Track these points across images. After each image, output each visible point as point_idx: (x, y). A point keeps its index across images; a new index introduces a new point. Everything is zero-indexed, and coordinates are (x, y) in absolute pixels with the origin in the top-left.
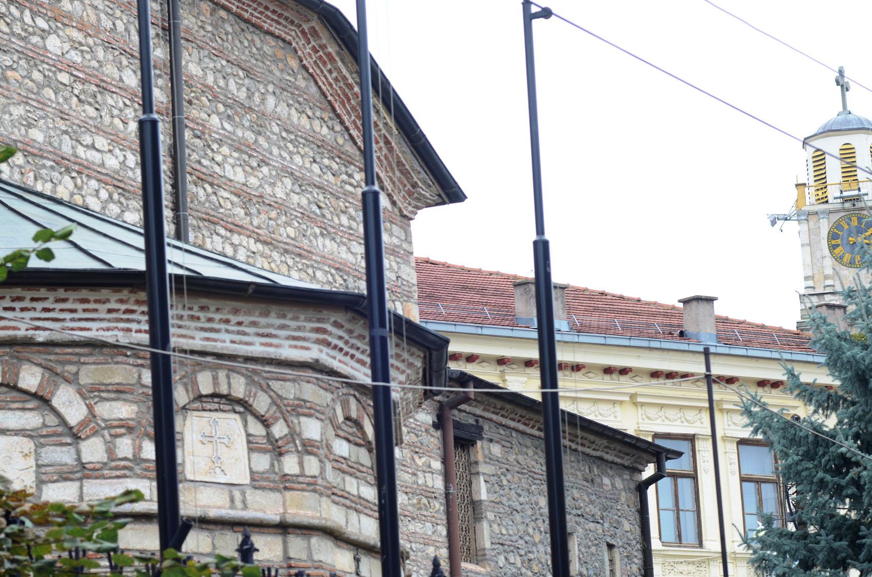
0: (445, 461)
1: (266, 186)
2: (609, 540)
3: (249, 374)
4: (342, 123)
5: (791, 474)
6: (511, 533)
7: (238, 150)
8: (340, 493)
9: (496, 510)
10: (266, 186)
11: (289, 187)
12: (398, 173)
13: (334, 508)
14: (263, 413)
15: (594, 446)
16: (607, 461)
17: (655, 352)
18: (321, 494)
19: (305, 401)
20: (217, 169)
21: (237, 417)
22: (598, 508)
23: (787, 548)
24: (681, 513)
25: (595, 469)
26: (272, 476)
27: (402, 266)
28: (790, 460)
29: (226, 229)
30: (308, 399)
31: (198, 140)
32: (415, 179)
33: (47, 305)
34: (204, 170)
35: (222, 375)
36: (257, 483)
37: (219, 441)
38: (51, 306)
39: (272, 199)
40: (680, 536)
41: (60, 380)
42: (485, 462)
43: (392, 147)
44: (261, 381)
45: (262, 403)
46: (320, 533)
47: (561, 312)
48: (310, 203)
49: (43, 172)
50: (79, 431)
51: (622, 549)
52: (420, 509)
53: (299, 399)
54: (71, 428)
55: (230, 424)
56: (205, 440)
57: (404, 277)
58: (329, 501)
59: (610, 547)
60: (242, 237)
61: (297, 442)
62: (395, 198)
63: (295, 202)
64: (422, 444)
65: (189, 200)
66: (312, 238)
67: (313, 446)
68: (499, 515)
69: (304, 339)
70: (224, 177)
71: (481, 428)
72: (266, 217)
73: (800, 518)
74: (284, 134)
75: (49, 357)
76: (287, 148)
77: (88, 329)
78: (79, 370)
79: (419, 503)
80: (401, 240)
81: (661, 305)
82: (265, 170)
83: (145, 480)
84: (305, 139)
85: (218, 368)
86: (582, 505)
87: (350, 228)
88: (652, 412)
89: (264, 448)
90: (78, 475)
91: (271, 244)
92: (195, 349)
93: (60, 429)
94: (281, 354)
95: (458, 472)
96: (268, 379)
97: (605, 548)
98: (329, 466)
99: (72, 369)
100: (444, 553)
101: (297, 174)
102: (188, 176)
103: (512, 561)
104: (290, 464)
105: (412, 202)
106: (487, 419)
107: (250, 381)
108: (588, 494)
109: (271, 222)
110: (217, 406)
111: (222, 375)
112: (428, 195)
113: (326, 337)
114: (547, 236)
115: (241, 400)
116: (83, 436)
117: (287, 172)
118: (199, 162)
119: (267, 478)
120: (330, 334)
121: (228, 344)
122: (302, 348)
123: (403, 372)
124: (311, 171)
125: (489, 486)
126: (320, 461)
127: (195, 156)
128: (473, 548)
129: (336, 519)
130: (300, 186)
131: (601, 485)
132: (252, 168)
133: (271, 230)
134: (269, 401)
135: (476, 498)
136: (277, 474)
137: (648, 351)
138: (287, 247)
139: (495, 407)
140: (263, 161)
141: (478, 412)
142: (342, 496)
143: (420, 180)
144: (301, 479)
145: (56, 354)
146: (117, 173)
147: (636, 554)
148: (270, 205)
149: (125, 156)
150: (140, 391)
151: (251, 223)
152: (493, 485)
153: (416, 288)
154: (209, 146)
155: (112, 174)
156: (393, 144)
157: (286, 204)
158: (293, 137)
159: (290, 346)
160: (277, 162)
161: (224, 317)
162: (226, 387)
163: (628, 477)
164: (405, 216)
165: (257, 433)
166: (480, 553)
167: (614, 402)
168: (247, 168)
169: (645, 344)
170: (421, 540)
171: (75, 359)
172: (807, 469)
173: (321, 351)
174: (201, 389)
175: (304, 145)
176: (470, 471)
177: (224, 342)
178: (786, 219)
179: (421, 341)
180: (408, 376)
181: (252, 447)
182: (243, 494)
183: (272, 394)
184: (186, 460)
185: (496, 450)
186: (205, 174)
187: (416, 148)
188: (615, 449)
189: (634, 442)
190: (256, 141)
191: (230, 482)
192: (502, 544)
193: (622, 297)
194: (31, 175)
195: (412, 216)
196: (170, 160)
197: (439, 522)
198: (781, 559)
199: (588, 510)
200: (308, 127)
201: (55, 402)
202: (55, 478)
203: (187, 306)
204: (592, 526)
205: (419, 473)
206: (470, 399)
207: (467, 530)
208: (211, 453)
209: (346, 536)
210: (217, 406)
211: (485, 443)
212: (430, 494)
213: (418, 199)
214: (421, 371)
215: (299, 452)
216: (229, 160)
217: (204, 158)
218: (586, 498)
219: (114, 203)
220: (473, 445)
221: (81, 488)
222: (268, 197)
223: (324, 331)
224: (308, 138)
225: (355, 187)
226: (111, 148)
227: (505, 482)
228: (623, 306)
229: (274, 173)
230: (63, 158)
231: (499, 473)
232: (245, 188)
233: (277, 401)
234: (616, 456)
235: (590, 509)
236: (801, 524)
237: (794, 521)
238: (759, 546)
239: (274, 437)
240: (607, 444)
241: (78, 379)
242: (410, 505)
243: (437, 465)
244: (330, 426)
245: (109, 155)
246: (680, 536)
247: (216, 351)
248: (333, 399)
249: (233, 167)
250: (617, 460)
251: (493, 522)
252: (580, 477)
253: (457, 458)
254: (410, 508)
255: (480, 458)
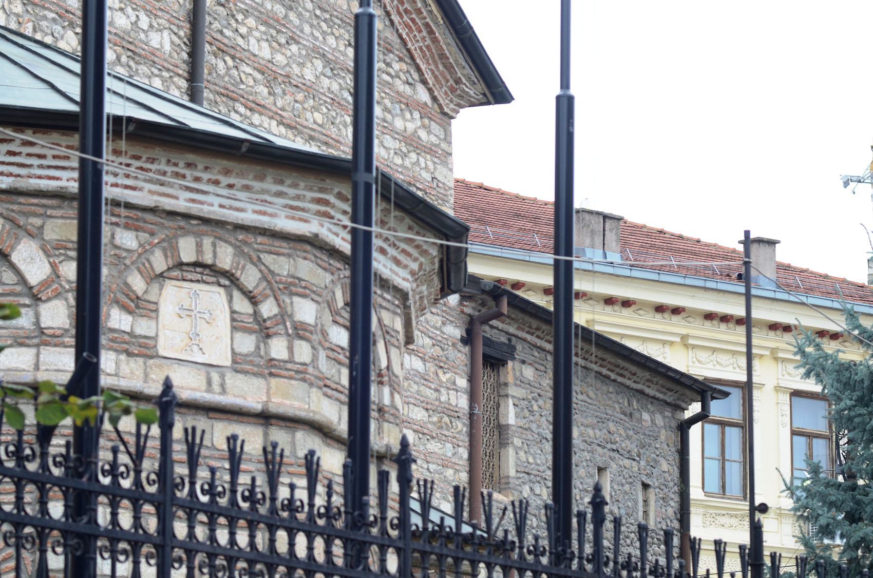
0: (472, 379)
1: (294, 66)
2: (644, 479)
3: (238, 244)
4: (418, 69)
5: (840, 421)
6: (539, 462)
7: (265, 23)
8: (334, 386)
9: (524, 436)
10: (294, 66)
11: (320, 69)
12: (441, 67)
13: (326, 402)
14: (251, 289)
15: (635, 378)
16: (648, 395)
17: (711, 292)
18: (311, 385)
19: (300, 279)
20: (240, 41)
21: (221, 290)
22: (635, 444)
23: (833, 498)
24: (727, 463)
25: (635, 403)
26: (257, 360)
27: (438, 167)
28: (842, 405)
29: (246, 107)
30: (303, 277)
31: (221, 8)
32: (459, 75)
33: (13, 147)
34: (226, 41)
35: (207, 242)
36: (238, 366)
37: (198, 315)
38: (17, 150)
39: (300, 80)
40: (723, 487)
41: (21, 233)
42: (516, 385)
43: (436, 38)
44: (251, 253)
45: (250, 277)
46: (307, 428)
47: (614, 244)
48: (341, 88)
49: (44, 24)
50: (39, 291)
51: (657, 490)
52: (441, 428)
53: (293, 277)
54: (31, 288)
55: (213, 298)
56: (184, 314)
57: (440, 178)
58: (320, 393)
59: (646, 486)
60: (263, 117)
61: (288, 324)
62: (436, 93)
63: (325, 86)
64: (447, 359)
65: (206, 71)
66: (341, 126)
67: (306, 330)
68: (527, 443)
69: (303, 210)
70: (248, 51)
71: (514, 348)
72: (292, 98)
73: (850, 469)
74: (318, 12)
75: (11, 207)
76: (320, 27)
77: (58, 179)
78: (44, 223)
79: (440, 422)
80: (440, 139)
81: (721, 247)
82: (294, 48)
83: (111, 352)
84: (341, 20)
85: (203, 235)
86: (618, 439)
87: (385, 120)
88: (703, 355)
89: (250, 328)
90: (36, 341)
91: (295, 128)
92: (178, 210)
93: (18, 288)
94: (276, 225)
95: (484, 391)
96: (259, 251)
97: (640, 487)
98: (322, 355)
99: (37, 222)
100: (464, 477)
101: (330, 56)
102: (207, 45)
103: (538, 491)
104: (278, 348)
105: (454, 99)
106: (520, 338)
107: (239, 252)
108: (626, 429)
109: (297, 105)
110: (199, 277)
111: (207, 242)
112: (472, 93)
113: (328, 209)
114: (573, 91)
115: (227, 272)
116: (43, 298)
117: (318, 53)
118: (221, 32)
119: (251, 361)
120: (333, 207)
121: (216, 208)
122: (301, 220)
123: (416, 260)
124: (345, 55)
125: (518, 410)
126: (313, 347)
127: (216, 25)
128: (496, 475)
129: (327, 414)
130: (332, 70)
131: (640, 420)
132: (280, 45)
133: (296, 113)
134: (259, 275)
135: (503, 421)
136: (261, 357)
137: (703, 291)
138: (313, 133)
139: (530, 327)
140: (292, 38)
141: (512, 330)
142: (336, 390)
143: (464, 76)
144: (289, 366)
145: (20, 204)
146: (129, 34)
147: (673, 496)
148: (297, 86)
149: (137, 16)
150: (113, 253)
151: (275, 104)
152: (522, 409)
153: (452, 192)
154: (233, 16)
155: (122, 34)
156: (437, 34)
157: (315, 87)
158: (328, 16)
159: (287, 217)
160: (308, 41)
161: (214, 177)
162: (211, 256)
163: (670, 415)
164: (446, 114)
165: (243, 310)
166: (503, 481)
167: (664, 343)
168: (274, 44)
169: (701, 283)
170: (440, 462)
171: (41, 211)
172: (860, 415)
173: (322, 226)
174: (182, 256)
175: (339, 26)
176: (498, 392)
177: (212, 205)
178: (860, 181)
179: (436, 225)
180: (421, 265)
181: (236, 324)
182: (222, 376)
183: (263, 268)
184: (160, 334)
185: (528, 372)
186: (227, 46)
187: (461, 40)
188: (657, 384)
189: (678, 377)
190: (286, 16)
191: (208, 362)
192: (528, 474)
193: (681, 237)
194: (30, 25)
195: (453, 114)
196: (188, 26)
197: (460, 443)
198: (825, 509)
199: (623, 445)
200: (345, 7)
201: (15, 258)
202: (9, 342)
203: (173, 161)
204: (627, 462)
205: (442, 390)
206: (503, 314)
207: (492, 455)
208: (189, 329)
209: (337, 433)
210: (199, 277)
211: (517, 364)
212: (453, 414)
213: (460, 97)
214: (437, 261)
215: (289, 335)
216: (254, 33)
217: (226, 28)
218: (622, 432)
219: (122, 66)
220: (503, 366)
221: (38, 355)
222: (295, 77)
223: (327, 203)
224: (345, 19)
225: (392, 77)
226: (123, 6)
227: (536, 408)
228: (680, 245)
229: (304, 52)
230: (67, 11)
231: (530, 397)
232: (270, 65)
233: (268, 276)
234: (658, 390)
235: (626, 445)
236: (851, 476)
237: (843, 473)
238: (804, 494)
239: (262, 316)
240: (649, 377)
241: (42, 234)
242: (430, 422)
243: (463, 383)
244: (327, 310)
245: (119, 13)
246: (723, 487)
247: (202, 215)
248: (333, 281)
249: (258, 41)
250: (661, 396)
251: (520, 448)
252: (618, 410)
253: (485, 377)
254: (429, 426)
255: (510, 379)
